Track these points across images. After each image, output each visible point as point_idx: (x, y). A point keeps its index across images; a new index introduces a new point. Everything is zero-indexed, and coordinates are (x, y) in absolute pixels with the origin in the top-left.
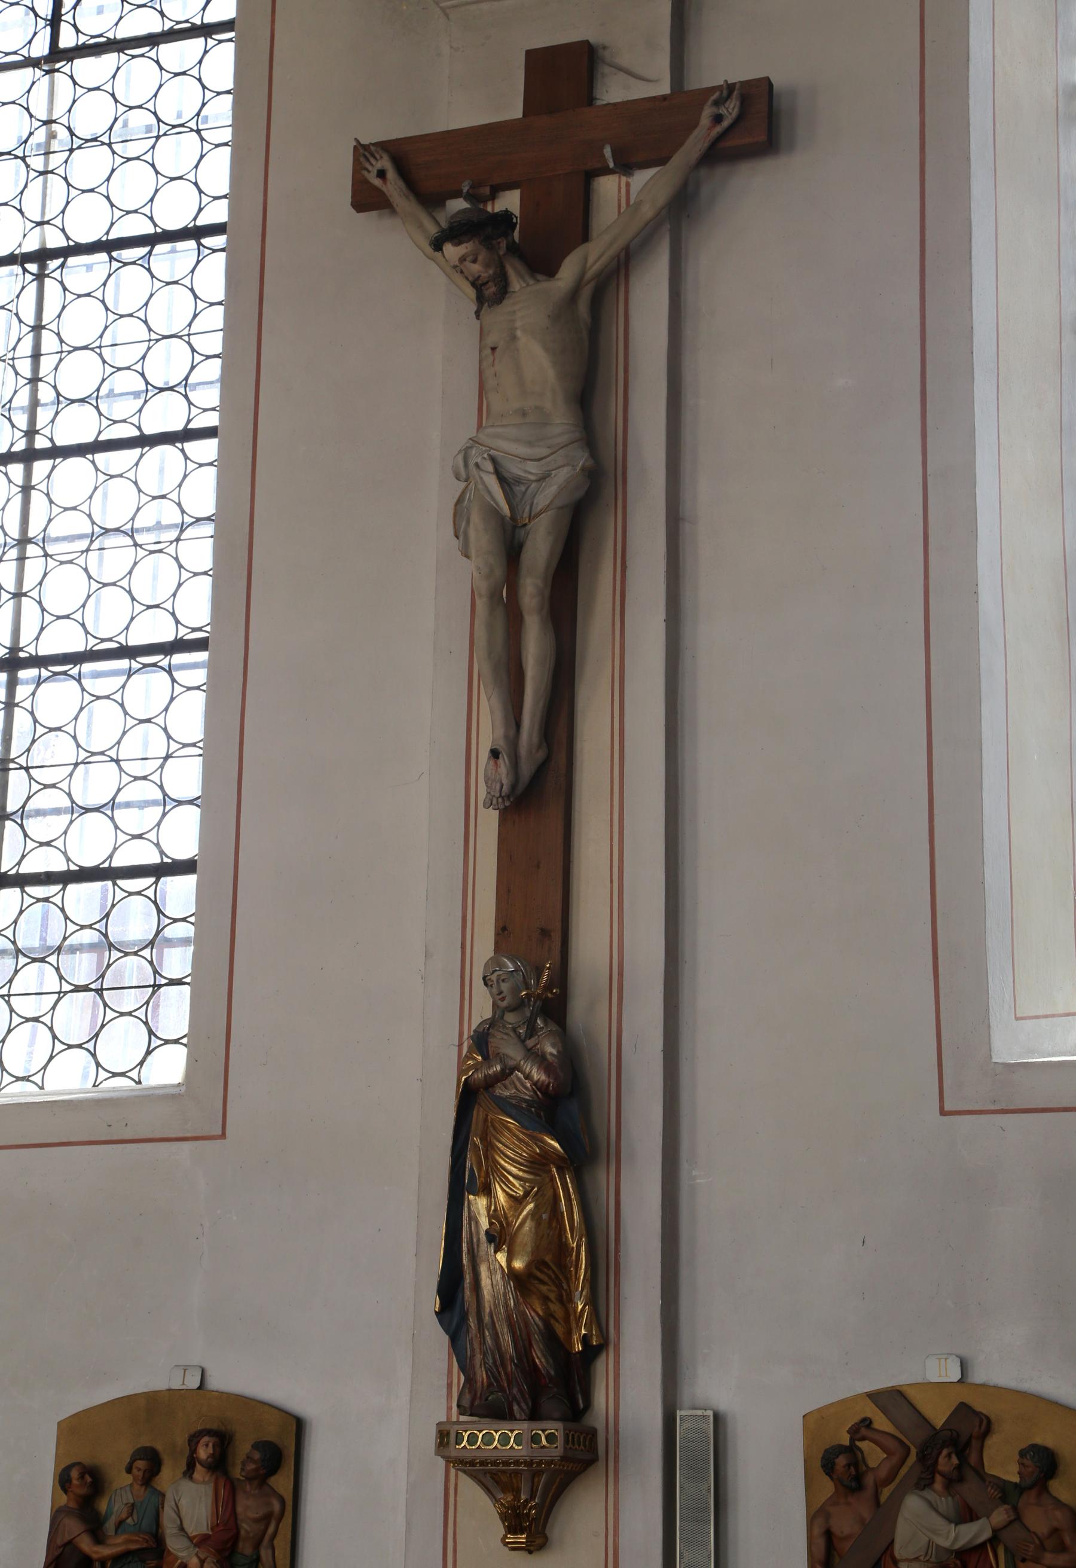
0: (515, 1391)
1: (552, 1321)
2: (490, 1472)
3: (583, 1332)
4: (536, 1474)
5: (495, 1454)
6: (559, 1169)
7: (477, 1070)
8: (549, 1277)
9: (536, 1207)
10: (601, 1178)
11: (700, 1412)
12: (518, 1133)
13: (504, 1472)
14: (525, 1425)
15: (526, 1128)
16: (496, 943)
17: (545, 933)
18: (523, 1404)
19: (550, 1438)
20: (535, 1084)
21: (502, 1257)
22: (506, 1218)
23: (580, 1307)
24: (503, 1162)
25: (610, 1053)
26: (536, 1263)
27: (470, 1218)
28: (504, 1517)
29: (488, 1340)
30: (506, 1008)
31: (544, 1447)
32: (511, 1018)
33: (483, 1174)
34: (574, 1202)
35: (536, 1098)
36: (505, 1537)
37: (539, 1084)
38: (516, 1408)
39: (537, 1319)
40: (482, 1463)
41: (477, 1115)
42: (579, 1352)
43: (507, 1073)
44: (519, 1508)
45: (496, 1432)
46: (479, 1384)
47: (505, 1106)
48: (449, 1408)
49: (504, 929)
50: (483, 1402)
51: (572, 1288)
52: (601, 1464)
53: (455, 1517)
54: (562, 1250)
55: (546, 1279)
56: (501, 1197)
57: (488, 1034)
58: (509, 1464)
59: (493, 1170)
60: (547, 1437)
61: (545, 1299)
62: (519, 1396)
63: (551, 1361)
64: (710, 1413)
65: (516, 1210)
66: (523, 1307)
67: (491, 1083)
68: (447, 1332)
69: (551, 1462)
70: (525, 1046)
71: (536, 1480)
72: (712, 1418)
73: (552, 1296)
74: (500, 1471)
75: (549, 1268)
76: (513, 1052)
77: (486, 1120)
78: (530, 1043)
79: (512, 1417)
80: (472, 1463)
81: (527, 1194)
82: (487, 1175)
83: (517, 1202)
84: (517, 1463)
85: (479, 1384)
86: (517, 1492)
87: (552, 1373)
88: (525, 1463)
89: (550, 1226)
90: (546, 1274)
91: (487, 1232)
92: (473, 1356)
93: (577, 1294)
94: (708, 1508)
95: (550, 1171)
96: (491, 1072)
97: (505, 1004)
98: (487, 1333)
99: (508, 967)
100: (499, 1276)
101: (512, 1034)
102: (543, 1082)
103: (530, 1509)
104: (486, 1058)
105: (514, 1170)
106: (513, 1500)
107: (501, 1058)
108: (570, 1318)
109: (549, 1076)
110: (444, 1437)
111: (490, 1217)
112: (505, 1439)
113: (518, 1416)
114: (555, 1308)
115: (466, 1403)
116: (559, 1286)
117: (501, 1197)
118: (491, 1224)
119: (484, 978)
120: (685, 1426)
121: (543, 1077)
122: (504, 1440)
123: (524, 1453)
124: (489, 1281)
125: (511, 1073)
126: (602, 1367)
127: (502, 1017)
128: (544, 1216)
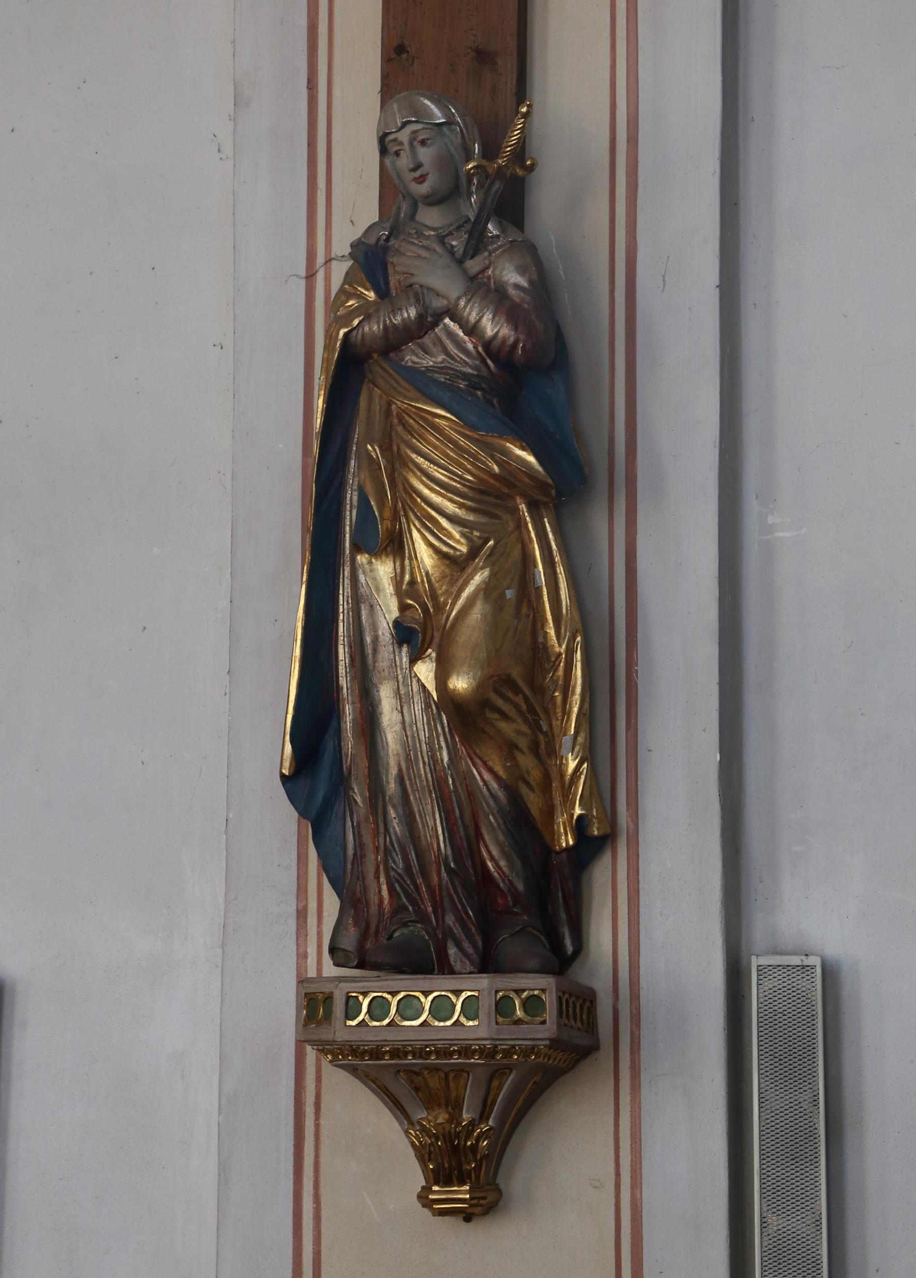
0: (450, 920)
1: (524, 790)
2: (411, 1072)
3: (578, 811)
4: (498, 1073)
5: (426, 1035)
6: (533, 506)
7: (367, 318)
8: (517, 707)
9: (492, 575)
10: (600, 524)
11: (795, 960)
12: (455, 436)
13: (436, 1069)
14: (484, 981)
15: (473, 428)
16: (385, 77)
17: (484, 57)
18: (466, 945)
19: (533, 1005)
20: (488, 345)
21: (425, 671)
22: (434, 596)
23: (572, 765)
24: (426, 492)
25: (612, 290)
26: (497, 683)
27: (357, 599)
28: (423, 1154)
29: (396, 826)
30: (427, 197)
31: (519, 1022)
32: (431, 217)
33: (387, 513)
34: (560, 570)
35: (485, 373)
36: (426, 1189)
37: (496, 343)
38: (452, 951)
39: (494, 785)
40: (396, 1053)
41: (368, 402)
42: (568, 849)
43: (427, 322)
44: (457, 1135)
45: (426, 994)
46: (374, 909)
47: (424, 384)
48: (302, 956)
49: (401, 49)
50: (381, 943)
51: (556, 730)
52: (605, 1054)
53: (317, 1157)
54: (538, 656)
55: (512, 712)
56: (426, 557)
57: (386, 249)
58: (451, 1054)
59: (406, 503)
60: (525, 1004)
61: (510, 749)
62: (457, 931)
63: (518, 864)
64: (815, 961)
65: (453, 582)
66: (466, 763)
67: (394, 342)
68: (303, 813)
69: (532, 1050)
70: (465, 271)
71: (495, 1083)
72: (819, 970)
73: (523, 743)
74: (428, 1068)
75: (517, 690)
76: (442, 281)
77: (388, 413)
78: (474, 266)
79: (445, 968)
80: (376, 1053)
81: (474, 552)
82: (395, 517)
83: (456, 565)
84: (465, 1052)
85: (374, 909)
86: (456, 1106)
87: (520, 886)
88: (482, 1051)
89: (518, 614)
90: (509, 705)
91: (397, 624)
92: (360, 857)
93: (567, 741)
94: (814, 1135)
95: (516, 510)
96: (397, 320)
97: (423, 189)
98: (392, 813)
99: (432, 115)
100: (418, 707)
101: (438, 248)
102: (504, 340)
103: (478, 1140)
104: (383, 293)
105: (450, 507)
106: (450, 1121)
107: (416, 293)
108: (551, 781)
109: (516, 328)
110: (315, 1006)
111: (399, 593)
112: (446, 1009)
113: (458, 967)
114: (526, 761)
115: (349, 941)
116: (535, 726)
117: (426, 557)
118: (403, 608)
119: (382, 140)
120: (767, 984)
121: (506, 331)
122: (441, 1009)
123: (482, 1033)
124: (396, 717)
125: (436, 324)
126: (603, 876)
127: (412, 217)
128: (509, 594)
